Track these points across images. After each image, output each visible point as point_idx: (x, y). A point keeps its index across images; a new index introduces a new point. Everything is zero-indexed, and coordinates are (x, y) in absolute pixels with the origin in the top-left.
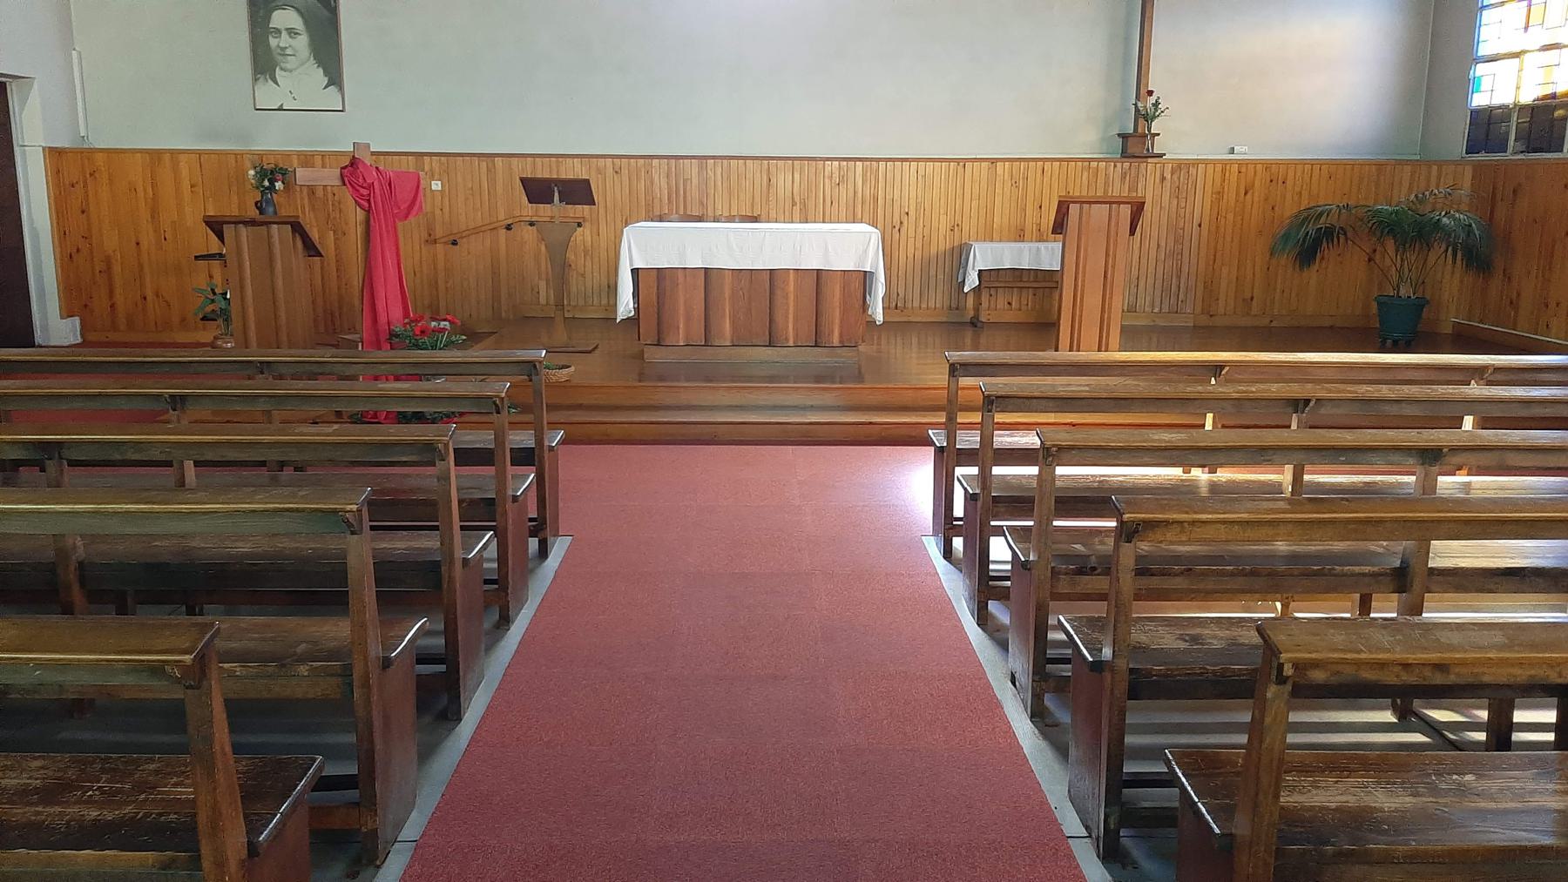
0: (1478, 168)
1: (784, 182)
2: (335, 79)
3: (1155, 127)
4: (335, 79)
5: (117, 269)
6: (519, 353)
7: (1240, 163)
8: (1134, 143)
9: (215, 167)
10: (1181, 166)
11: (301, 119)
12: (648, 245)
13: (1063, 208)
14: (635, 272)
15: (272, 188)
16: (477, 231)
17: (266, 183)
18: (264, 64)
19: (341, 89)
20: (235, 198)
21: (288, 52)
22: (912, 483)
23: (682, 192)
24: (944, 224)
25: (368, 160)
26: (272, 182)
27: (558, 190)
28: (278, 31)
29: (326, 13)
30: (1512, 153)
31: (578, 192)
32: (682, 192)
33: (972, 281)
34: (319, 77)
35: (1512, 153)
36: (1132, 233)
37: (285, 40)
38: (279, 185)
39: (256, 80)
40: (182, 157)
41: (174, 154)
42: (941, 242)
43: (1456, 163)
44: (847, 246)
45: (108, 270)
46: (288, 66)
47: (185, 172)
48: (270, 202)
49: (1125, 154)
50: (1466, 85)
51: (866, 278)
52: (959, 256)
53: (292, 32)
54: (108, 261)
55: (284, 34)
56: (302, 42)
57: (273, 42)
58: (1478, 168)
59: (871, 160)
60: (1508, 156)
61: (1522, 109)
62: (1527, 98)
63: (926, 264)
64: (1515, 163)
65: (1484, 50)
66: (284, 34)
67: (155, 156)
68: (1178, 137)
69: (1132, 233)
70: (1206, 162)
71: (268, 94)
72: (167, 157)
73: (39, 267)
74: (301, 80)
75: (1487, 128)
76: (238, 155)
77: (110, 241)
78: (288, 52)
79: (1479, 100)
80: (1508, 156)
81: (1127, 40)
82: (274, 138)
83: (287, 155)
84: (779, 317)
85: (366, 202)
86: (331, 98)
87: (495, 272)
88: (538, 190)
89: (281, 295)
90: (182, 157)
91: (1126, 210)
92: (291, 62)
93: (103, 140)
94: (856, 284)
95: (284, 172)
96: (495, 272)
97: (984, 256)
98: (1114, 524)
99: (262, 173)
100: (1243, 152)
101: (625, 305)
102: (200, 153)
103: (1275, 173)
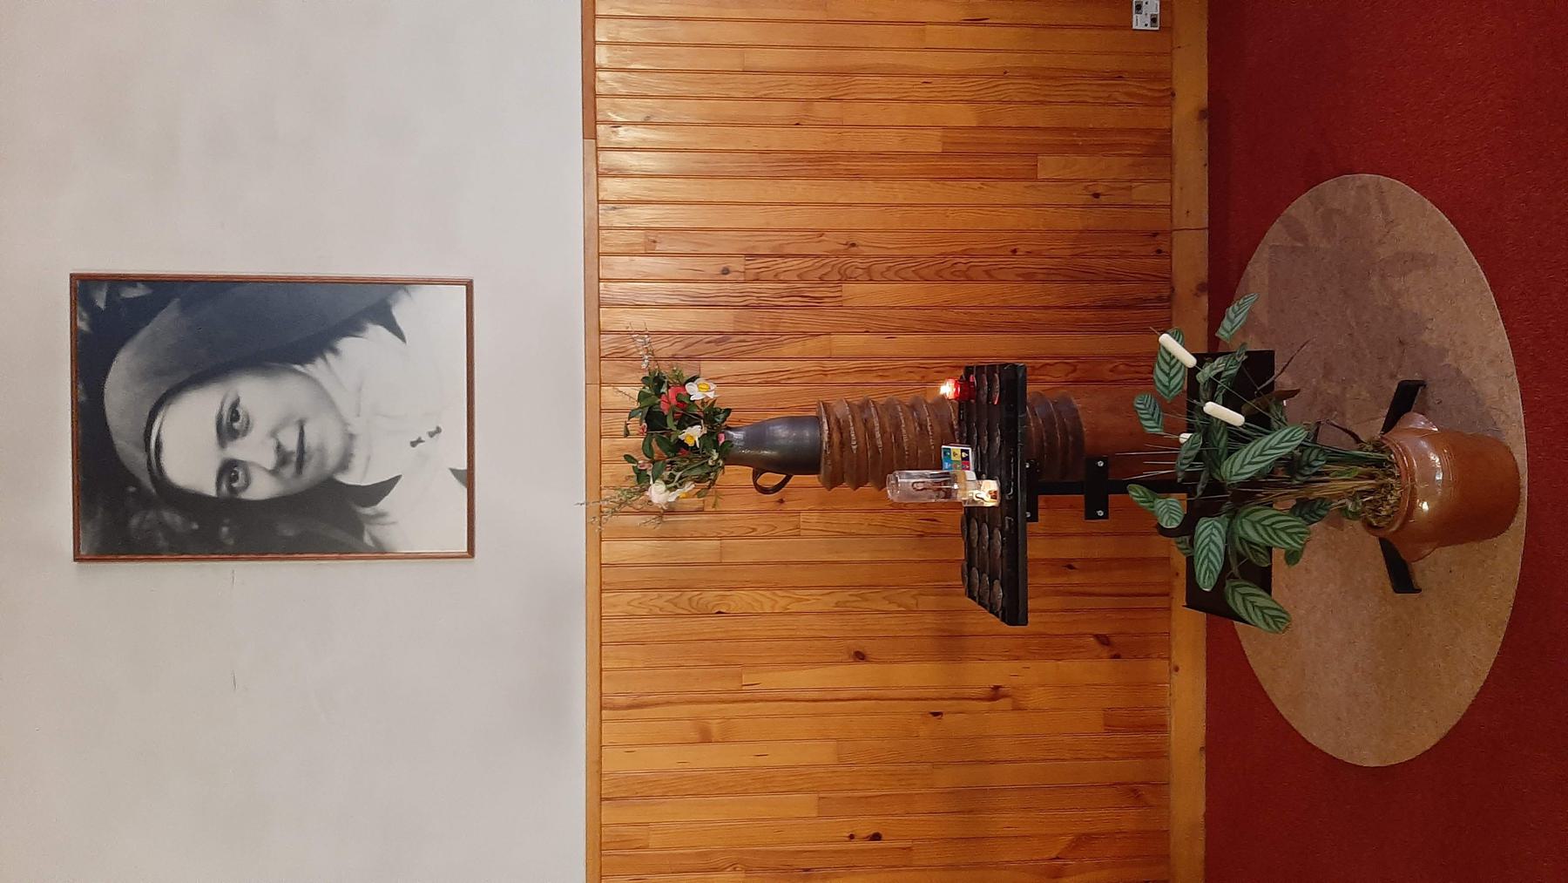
9: (650, 646)
11: (490, 426)
15: (712, 416)
17: (693, 434)
18: (320, 516)
19: (403, 285)
20: (741, 600)
21: (291, 444)
28: (229, 470)
29: (168, 318)
34: (362, 351)
37: (255, 450)
39: (380, 552)
40: (615, 762)
41: (601, 794)
46: (334, 447)
47: (664, 760)
53: (230, 427)
55: (237, 451)
56: (263, 398)
57: (261, 488)
59: (590, 68)
66: (237, 451)
71: (420, 514)
72: (609, 814)
78: (291, 444)
86: (431, 317)
90: (615, 762)
92: (323, 436)
98: (1166, 339)
102: (601, 706)
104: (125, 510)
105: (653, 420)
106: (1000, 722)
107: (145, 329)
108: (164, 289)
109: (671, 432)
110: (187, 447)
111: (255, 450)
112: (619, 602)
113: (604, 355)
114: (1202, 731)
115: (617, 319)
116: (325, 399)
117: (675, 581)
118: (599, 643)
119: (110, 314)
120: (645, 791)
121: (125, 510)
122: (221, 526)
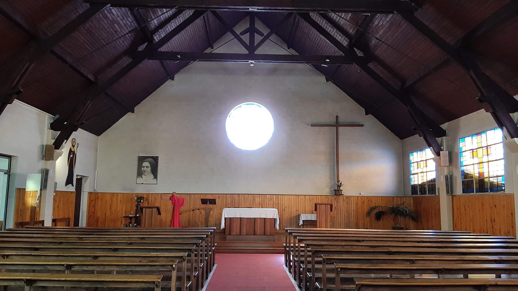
0: (414, 198)
1: (257, 199)
2: (156, 177)
3: (341, 188)
4: (156, 177)
5: (100, 220)
6: (146, 286)
7: (361, 197)
8: (337, 192)
9: (127, 197)
10: (348, 197)
11: (147, 186)
12: (228, 213)
13: (316, 205)
14: (225, 218)
15: (140, 201)
16: (186, 211)
18: (140, 174)
22: (282, 258)
23: (235, 201)
24: (294, 209)
25: (176, 195)
26: (140, 200)
27: (208, 201)
30: (419, 195)
31: (213, 202)
32: (235, 201)
33: (301, 223)
34: (152, 176)
35: (419, 195)
36: (331, 211)
37: (145, 169)
38: (142, 201)
41: (117, 194)
42: (294, 214)
43: (409, 197)
44: (271, 213)
45: (97, 221)
47: (119, 198)
48: (139, 205)
49: (336, 195)
50: (409, 180)
51: (275, 220)
52: (298, 217)
53: (147, 167)
54: (98, 218)
56: (149, 169)
57: (142, 169)
58: (414, 198)
60: (427, 195)
61: (420, 185)
62: (420, 183)
63: (291, 219)
64: (429, 197)
65: (503, 162)
67: (113, 194)
68: (347, 190)
69: (331, 211)
70: (353, 196)
71: (140, 180)
73: (82, 219)
74: (148, 177)
75: (414, 188)
76: (132, 194)
77: (99, 214)
79: (412, 183)
80: (427, 195)
81: (334, 170)
82: (141, 190)
83: (143, 194)
84: (256, 228)
85: (174, 204)
86: (154, 181)
87: (189, 221)
88: (204, 201)
89: (153, 223)
91: (329, 206)
92: (146, 173)
93: (98, 191)
94: (273, 221)
95: (143, 198)
96: (189, 221)
97: (303, 217)
99: (138, 198)
100: (363, 194)
101: (223, 226)
102: (123, 194)
103: (369, 199)
104: (141, 159)
105: (141, 198)
106: (120, 223)
107: (154, 162)
108: (157, 163)
109: (140, 198)
110: (146, 164)
111: (145, 169)
112: (131, 195)
113: (148, 195)
114: (68, 168)
115: (151, 195)
116: (149, 174)
117: (132, 199)
118: (128, 194)
119: (156, 159)
120: (117, 196)
121: (141, 159)
122: (140, 166)
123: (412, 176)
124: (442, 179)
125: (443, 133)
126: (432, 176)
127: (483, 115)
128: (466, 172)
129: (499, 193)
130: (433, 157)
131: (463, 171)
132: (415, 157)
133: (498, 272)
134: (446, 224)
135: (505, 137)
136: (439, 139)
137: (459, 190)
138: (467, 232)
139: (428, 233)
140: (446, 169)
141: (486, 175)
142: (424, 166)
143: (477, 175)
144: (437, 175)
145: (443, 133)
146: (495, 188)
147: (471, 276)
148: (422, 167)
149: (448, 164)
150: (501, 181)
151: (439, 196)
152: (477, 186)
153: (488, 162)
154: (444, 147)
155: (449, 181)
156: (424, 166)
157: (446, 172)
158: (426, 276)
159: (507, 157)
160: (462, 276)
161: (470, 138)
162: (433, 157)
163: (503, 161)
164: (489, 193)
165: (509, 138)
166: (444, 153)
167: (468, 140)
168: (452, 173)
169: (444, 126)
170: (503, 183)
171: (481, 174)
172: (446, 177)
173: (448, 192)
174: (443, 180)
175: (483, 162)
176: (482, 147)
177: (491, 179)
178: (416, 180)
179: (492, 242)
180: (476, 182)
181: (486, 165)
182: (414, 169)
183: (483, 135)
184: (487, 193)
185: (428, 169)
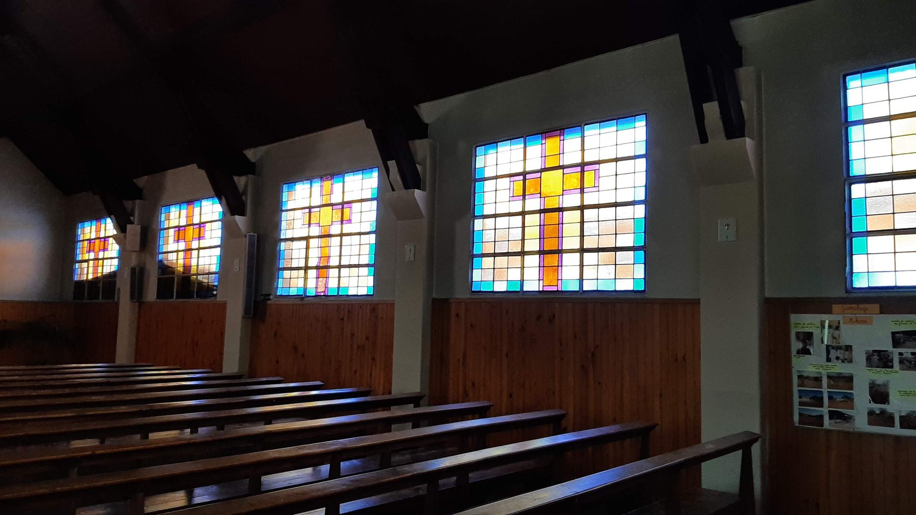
50: (72, 271)
79: (76, 278)
80: (85, 301)
123: (857, 191)
124: (126, 274)
125: (249, 168)
126: (111, 266)
127: (194, 174)
128: (166, 262)
129: (208, 300)
130: (115, 233)
131: (161, 261)
132: (88, 231)
133: (194, 425)
134: (124, 351)
135: (224, 214)
136: (128, 204)
137: (151, 294)
138: (156, 362)
139: (93, 370)
140: (134, 256)
141: (194, 270)
142: (100, 248)
143: (181, 269)
144: (120, 266)
145: (138, 194)
146: (206, 291)
147: (154, 436)
148: (97, 249)
149: (137, 248)
150: (213, 280)
151: (117, 304)
152: (181, 285)
153: (341, 235)
154: (136, 218)
155: (138, 276)
156: (100, 248)
157: (134, 261)
158: (77, 444)
159: (381, 229)
160: (138, 436)
161: (178, 207)
162: (115, 233)
163: (219, 249)
164: (195, 300)
165: (228, 215)
166: (134, 229)
167: (174, 211)
168: (145, 264)
169: (251, 154)
170: (216, 284)
171: (187, 268)
172: (133, 270)
173: (132, 296)
174: (127, 275)
175: (330, 236)
176: (332, 205)
177: (200, 278)
178: (86, 272)
179: (188, 378)
180: (178, 280)
181: (335, 241)
182: (83, 253)
183: (197, 204)
184: (192, 300)
185: (107, 254)
